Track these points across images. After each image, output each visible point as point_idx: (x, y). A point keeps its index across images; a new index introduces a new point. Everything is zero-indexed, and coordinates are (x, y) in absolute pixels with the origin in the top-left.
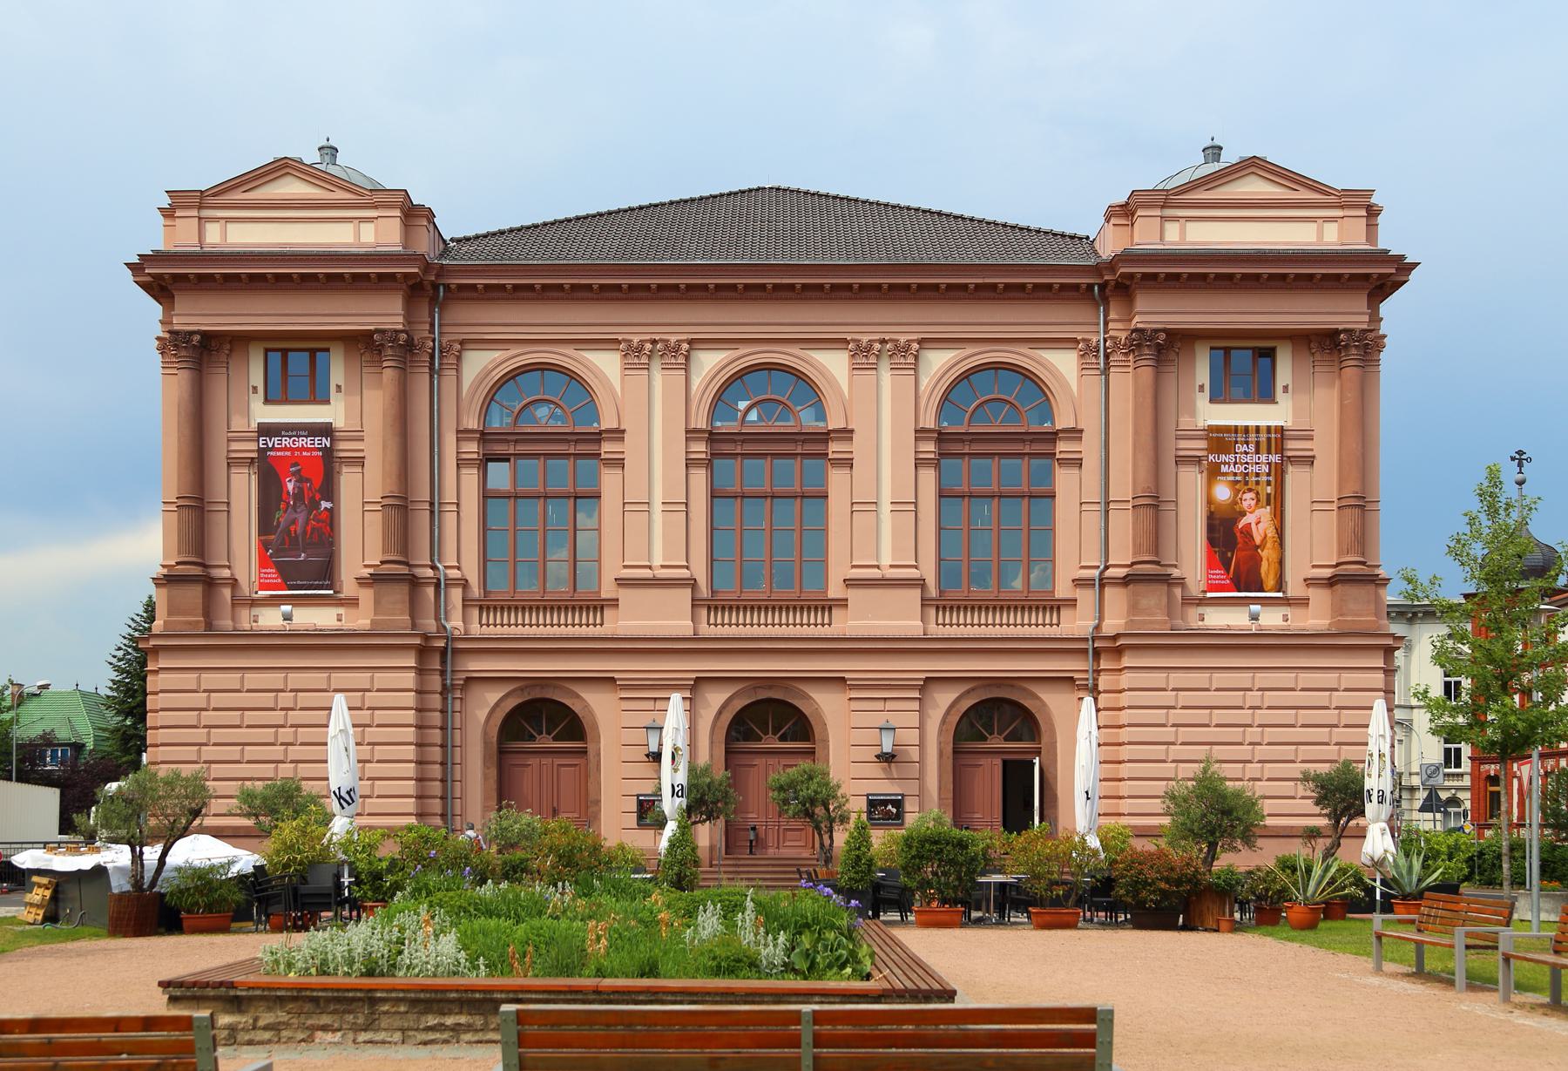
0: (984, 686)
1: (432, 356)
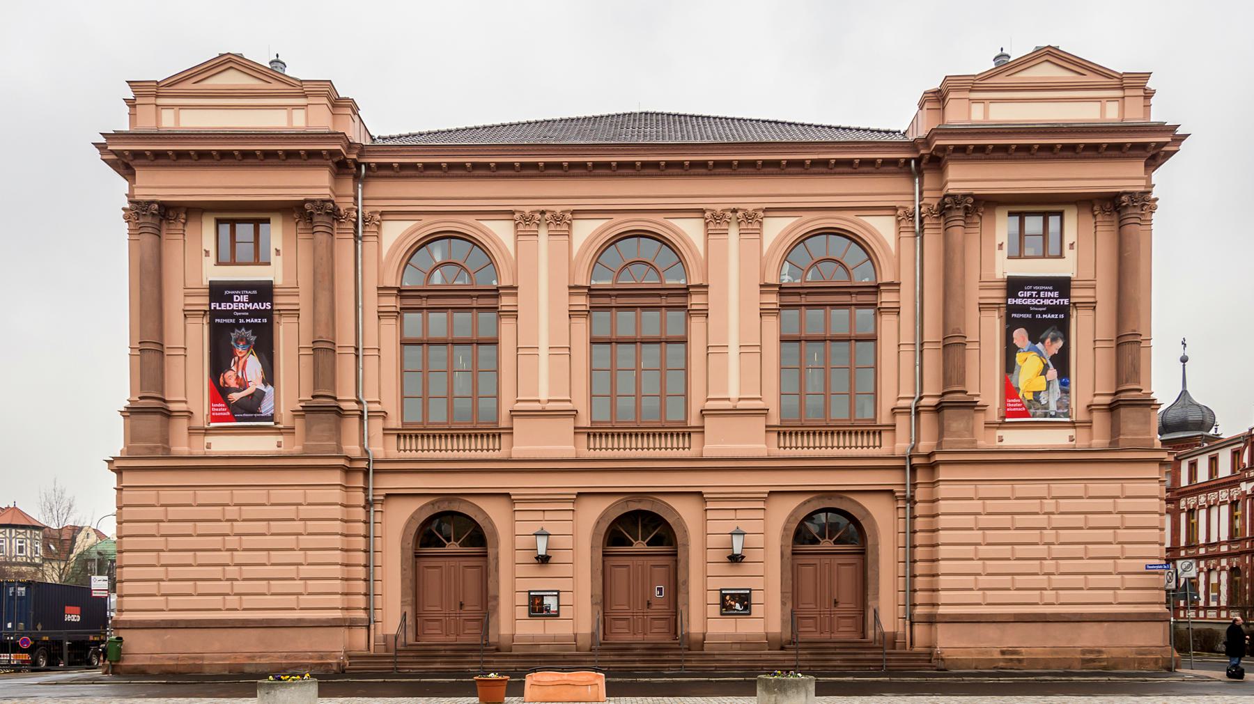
0: (818, 498)
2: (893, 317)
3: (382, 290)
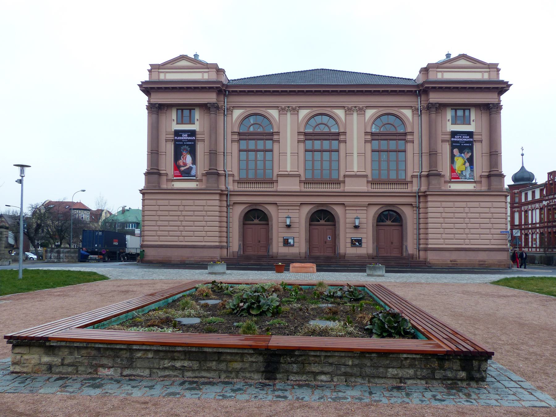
1: (224, 111)
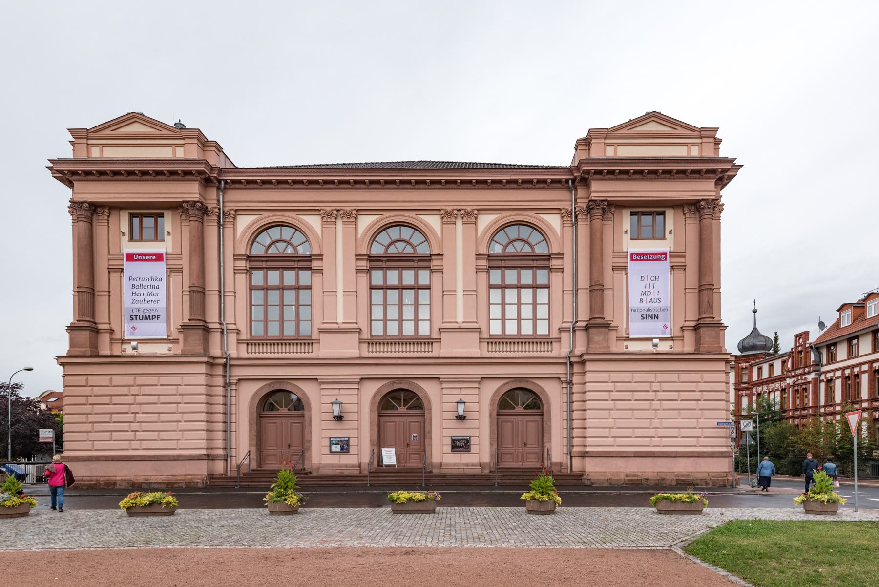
2: (560, 274)
3: (236, 257)
